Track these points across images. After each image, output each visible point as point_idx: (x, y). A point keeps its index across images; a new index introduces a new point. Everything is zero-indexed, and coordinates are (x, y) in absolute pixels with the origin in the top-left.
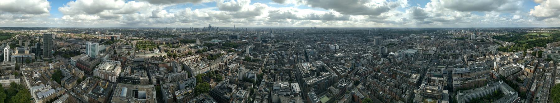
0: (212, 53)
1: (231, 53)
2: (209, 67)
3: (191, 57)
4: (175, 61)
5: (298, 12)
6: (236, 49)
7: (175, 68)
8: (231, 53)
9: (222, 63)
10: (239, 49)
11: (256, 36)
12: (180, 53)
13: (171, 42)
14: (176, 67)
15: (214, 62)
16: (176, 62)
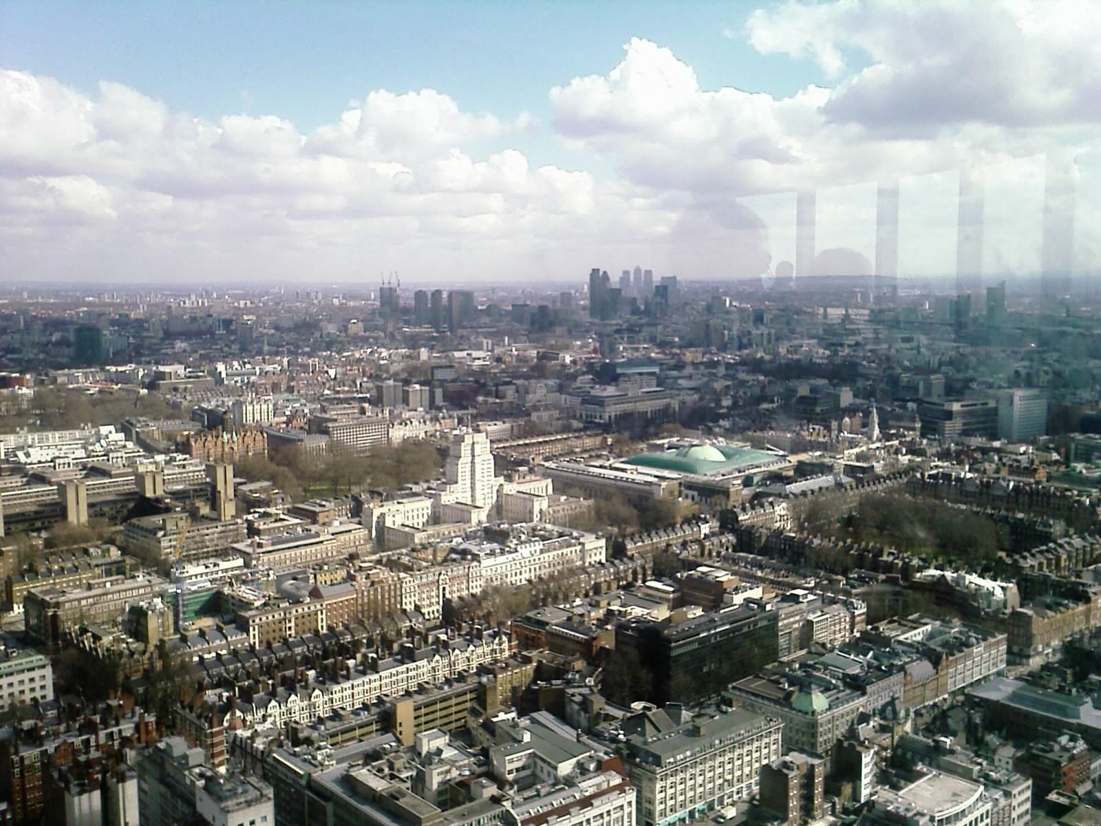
0: (661, 613)
1: (917, 635)
2: (632, 796)
4: (178, 744)
8: (917, 635)
12: (243, 627)
15: (694, 732)
16: (196, 755)
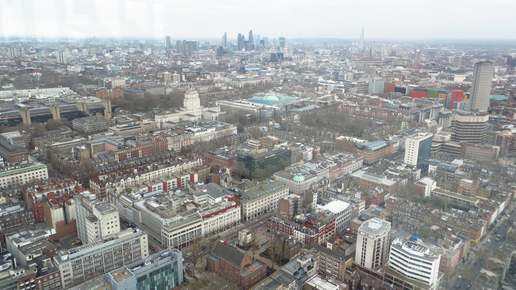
2: (239, 209)
3: (163, 171)
5: (251, 31)
6: (359, 141)
7: (88, 222)
9: (292, 196)
10: (371, 140)
11: (465, 88)
13: (62, 109)
14: (94, 219)
